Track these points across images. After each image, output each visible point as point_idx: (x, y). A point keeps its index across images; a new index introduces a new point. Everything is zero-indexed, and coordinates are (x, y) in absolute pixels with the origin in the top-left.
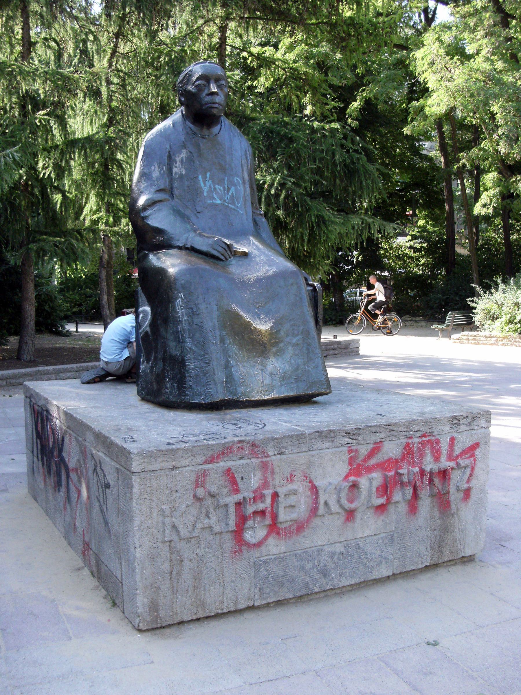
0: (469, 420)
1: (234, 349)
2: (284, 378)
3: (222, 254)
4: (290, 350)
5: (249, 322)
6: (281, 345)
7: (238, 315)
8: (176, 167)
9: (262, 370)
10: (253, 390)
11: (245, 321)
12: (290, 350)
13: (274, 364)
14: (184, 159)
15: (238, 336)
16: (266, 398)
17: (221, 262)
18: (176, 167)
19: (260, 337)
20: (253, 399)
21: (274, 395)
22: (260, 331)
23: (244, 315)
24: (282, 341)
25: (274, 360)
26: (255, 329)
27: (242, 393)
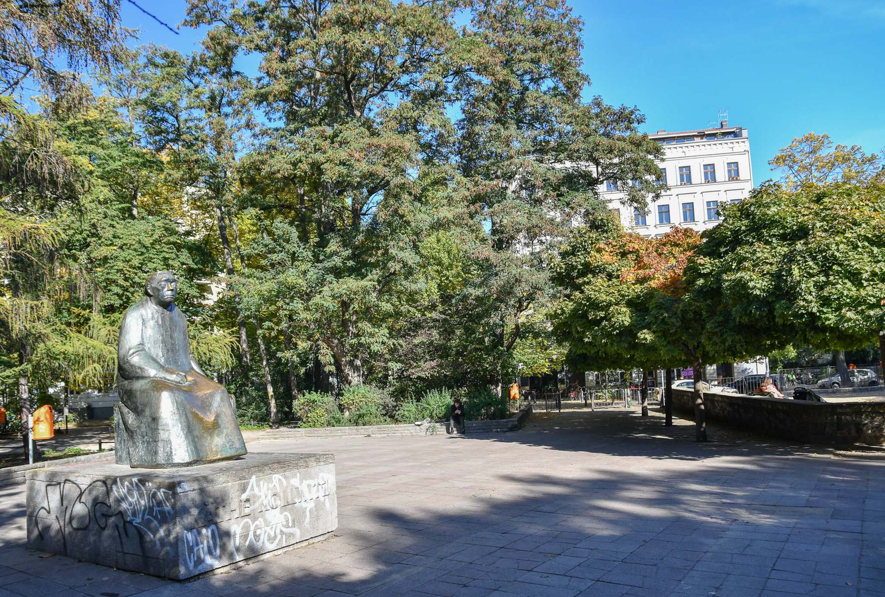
2: (224, 446)
21: (219, 457)
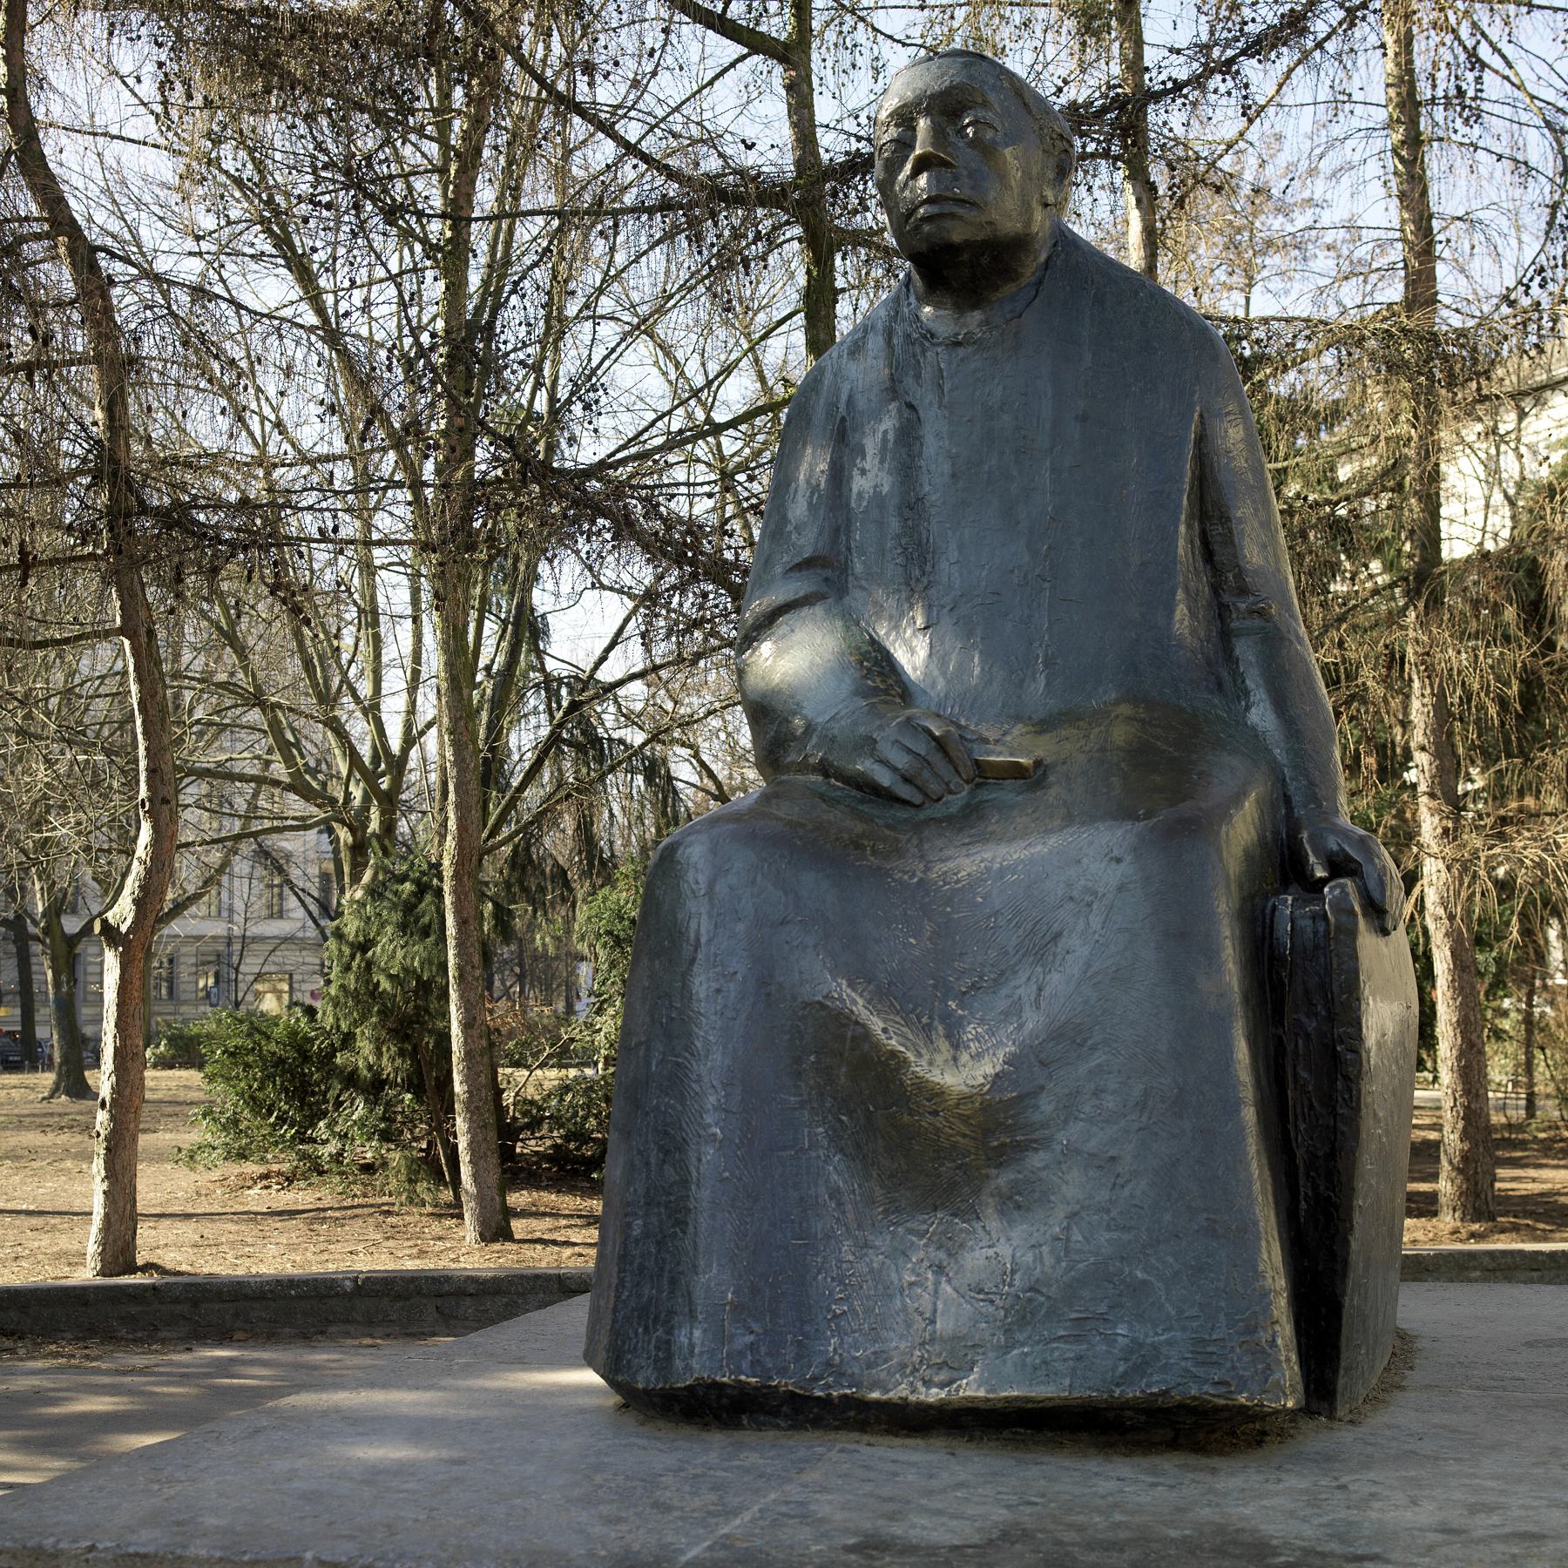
1: (836, 1172)
2: (1025, 1312)
3: (907, 780)
4: (1073, 1186)
5: (893, 1054)
6: (1037, 1160)
8: (863, 472)
9: (939, 1269)
11: (877, 1046)
12: (1073, 1186)
13: (999, 1248)
14: (891, 436)
15: (850, 1113)
16: (934, 1395)
17: (903, 814)
18: (863, 472)
19: (939, 1121)
20: (875, 1395)
21: (971, 1388)
22: (937, 1094)
23: (876, 1024)
24: (1045, 1143)
25: (994, 1224)
26: (921, 1085)
27: (829, 1363)
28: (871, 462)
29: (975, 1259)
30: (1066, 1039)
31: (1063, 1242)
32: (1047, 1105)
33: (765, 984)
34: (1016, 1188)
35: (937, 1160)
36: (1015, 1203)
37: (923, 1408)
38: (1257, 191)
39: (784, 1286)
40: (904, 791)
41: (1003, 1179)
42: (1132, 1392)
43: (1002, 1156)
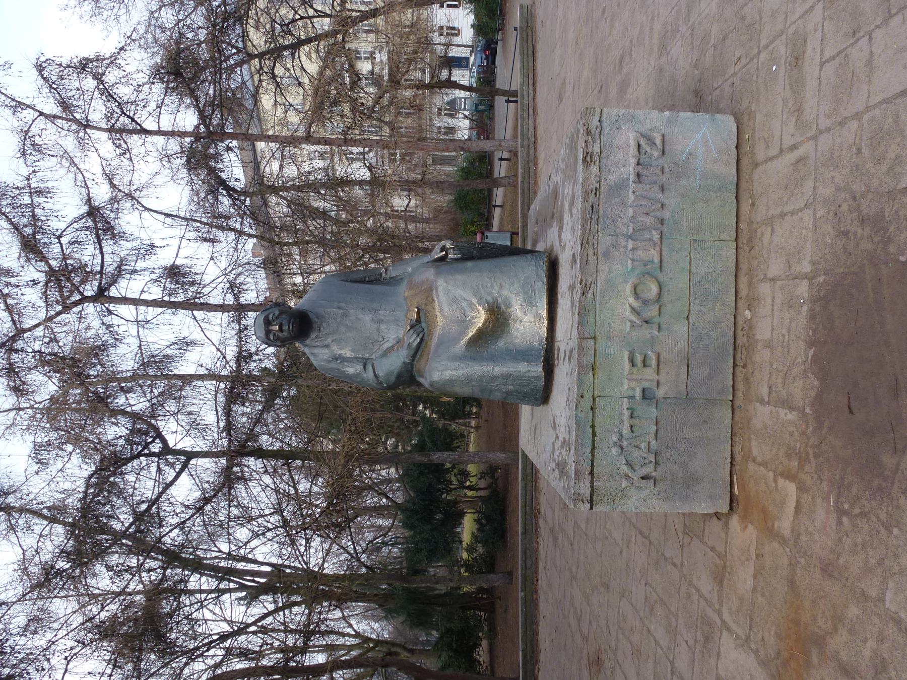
0: (590, 140)
1: (501, 344)
2: (530, 302)
4: (505, 292)
6: (500, 300)
7: (470, 339)
10: (538, 333)
12: (505, 292)
13: (517, 308)
16: (546, 322)
17: (426, 337)
21: (544, 314)
23: (471, 334)
24: (497, 299)
25: (512, 309)
28: (343, 352)
29: (519, 314)
30: (476, 293)
31: (517, 294)
32: (489, 298)
33: (461, 358)
34: (505, 305)
35: (498, 319)
36: (509, 305)
37: (548, 323)
38: (690, 154)
39: (523, 355)
40: (421, 335)
41: (503, 307)
42: (545, 280)
43: (499, 308)
